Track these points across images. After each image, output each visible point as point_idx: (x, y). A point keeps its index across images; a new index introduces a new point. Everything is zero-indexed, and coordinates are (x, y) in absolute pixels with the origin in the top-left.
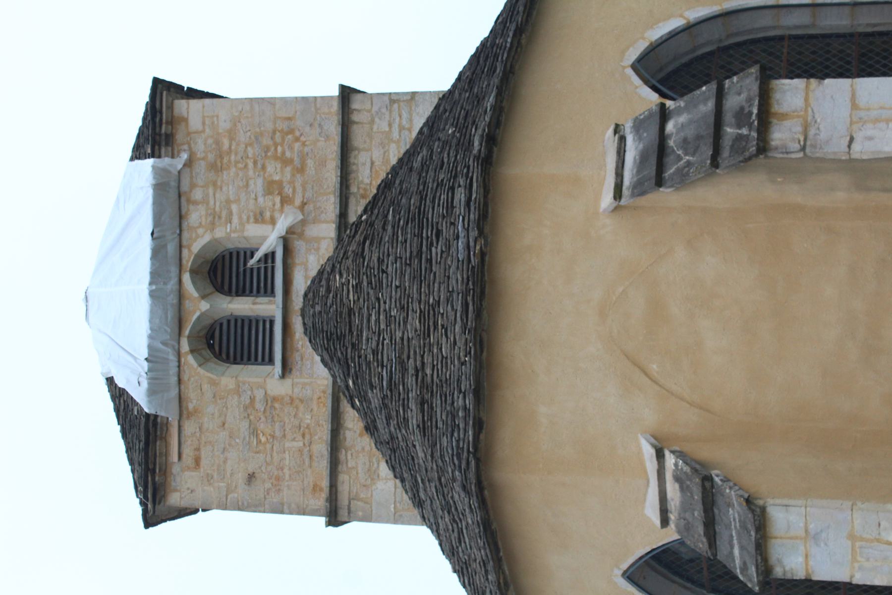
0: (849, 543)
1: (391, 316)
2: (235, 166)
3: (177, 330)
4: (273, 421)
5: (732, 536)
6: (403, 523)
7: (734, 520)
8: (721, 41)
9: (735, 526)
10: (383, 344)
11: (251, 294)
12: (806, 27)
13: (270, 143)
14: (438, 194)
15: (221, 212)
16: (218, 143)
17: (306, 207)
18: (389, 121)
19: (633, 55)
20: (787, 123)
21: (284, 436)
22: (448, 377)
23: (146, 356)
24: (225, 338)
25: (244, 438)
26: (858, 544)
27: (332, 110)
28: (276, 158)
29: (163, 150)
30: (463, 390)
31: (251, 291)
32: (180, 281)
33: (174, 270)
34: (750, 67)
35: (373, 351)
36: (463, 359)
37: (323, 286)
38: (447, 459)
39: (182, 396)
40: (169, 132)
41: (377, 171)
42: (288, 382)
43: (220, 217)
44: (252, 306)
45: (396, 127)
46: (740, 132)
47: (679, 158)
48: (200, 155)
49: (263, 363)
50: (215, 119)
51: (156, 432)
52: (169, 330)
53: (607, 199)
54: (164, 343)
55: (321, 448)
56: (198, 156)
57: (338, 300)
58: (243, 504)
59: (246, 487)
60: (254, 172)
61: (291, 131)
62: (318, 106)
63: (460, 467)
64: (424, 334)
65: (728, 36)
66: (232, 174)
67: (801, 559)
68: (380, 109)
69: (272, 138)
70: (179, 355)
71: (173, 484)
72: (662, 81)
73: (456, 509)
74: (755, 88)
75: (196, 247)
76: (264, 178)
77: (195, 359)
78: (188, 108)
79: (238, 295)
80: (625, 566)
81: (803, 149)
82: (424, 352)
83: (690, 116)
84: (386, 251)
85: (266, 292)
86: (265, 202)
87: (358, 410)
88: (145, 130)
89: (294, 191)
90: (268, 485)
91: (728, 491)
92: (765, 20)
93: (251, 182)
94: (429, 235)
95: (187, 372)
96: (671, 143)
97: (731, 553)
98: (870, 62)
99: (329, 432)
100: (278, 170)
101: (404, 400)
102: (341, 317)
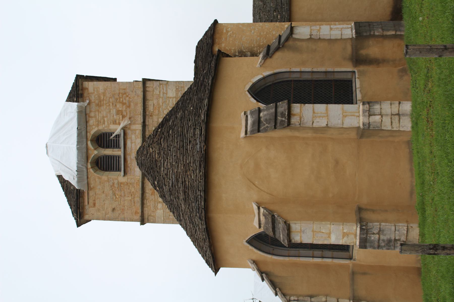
0: (312, 233)
1: (172, 164)
2: (106, 105)
3: (86, 161)
4: (121, 191)
5: (280, 232)
6: (166, 223)
7: (281, 227)
8: (273, 81)
10: (169, 173)
11: (111, 148)
12: (298, 78)
13: (118, 97)
14: (189, 130)
15: (101, 120)
16: (99, 97)
17: (131, 119)
18: (159, 91)
19: (248, 87)
20: (295, 117)
21: (125, 196)
22: (194, 185)
23: (76, 170)
24: (102, 163)
25: (111, 197)
26: (315, 233)
27: (139, 87)
28: (120, 102)
30: (200, 190)
31: (111, 147)
32: (87, 144)
33: (85, 140)
34: (285, 100)
35: (166, 174)
36: (200, 181)
37: (145, 151)
38: (194, 210)
39: (89, 183)
40: (82, 93)
41: (155, 107)
42: (126, 178)
43: (101, 122)
44: (112, 152)
45: (162, 93)
46: (282, 119)
47: (264, 125)
48: (93, 101)
49: (116, 171)
50: (98, 89)
51: (80, 195)
52: (84, 161)
53: (243, 134)
54: (82, 165)
55: (138, 199)
56: (92, 101)
57: (151, 156)
58: (111, 218)
59: (112, 213)
60: (112, 107)
61: (125, 93)
62: (134, 85)
63: (199, 212)
64: (185, 171)
65: (275, 80)
66: (104, 108)
67: (299, 238)
68: (156, 87)
69: (118, 96)
70: (87, 169)
71: (86, 212)
72: (255, 95)
73: (196, 224)
74: (286, 107)
75: (92, 132)
76: (116, 109)
77: (93, 170)
78: (88, 85)
79: (106, 148)
80: (247, 239)
81: (300, 124)
82: (185, 177)
83: (267, 112)
84: (170, 144)
85: (116, 147)
86: (116, 117)
88: (73, 92)
90: (120, 212)
91: (279, 219)
92: (286, 75)
93: (111, 110)
94: (187, 141)
95: (90, 174)
96: (262, 119)
97: (280, 236)
98: (317, 90)
99: (141, 194)
100: (121, 106)
101: (178, 190)
102: (152, 162)
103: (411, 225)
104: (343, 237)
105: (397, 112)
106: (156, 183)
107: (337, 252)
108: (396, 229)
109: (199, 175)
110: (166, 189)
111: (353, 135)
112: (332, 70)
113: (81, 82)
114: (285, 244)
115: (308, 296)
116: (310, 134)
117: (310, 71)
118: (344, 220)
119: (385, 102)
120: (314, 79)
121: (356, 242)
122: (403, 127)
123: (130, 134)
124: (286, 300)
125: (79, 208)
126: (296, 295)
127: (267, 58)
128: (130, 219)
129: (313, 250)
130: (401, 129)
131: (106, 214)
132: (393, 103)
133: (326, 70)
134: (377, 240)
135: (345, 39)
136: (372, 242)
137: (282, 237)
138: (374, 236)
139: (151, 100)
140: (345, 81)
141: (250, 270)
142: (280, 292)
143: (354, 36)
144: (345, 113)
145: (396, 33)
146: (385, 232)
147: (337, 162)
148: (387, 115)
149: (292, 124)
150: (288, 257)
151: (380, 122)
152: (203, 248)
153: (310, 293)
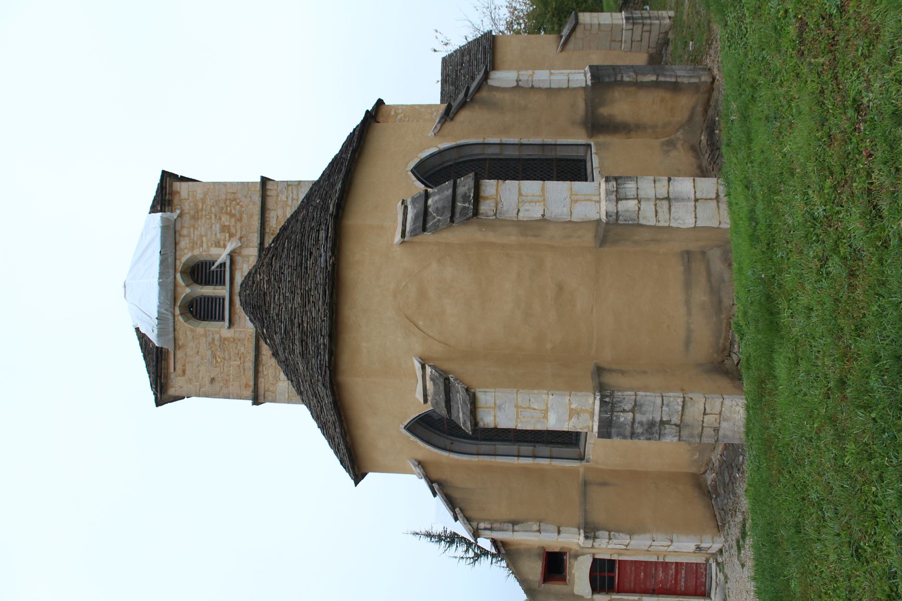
2: (205, 217)
4: (224, 351)
8: (456, 159)
9: (460, 402)
11: (212, 284)
13: (224, 205)
16: (196, 205)
19: (412, 165)
20: (488, 202)
21: (230, 358)
23: (157, 316)
26: (520, 410)
28: (226, 213)
29: (167, 209)
31: (213, 283)
33: (172, 271)
34: (470, 173)
35: (277, 314)
40: (170, 199)
41: (280, 221)
42: (232, 330)
43: (197, 244)
45: (290, 198)
47: (434, 218)
48: (186, 211)
53: (398, 238)
54: (166, 310)
55: (250, 365)
61: (235, 200)
66: (203, 221)
67: (492, 418)
68: (282, 189)
70: (174, 316)
71: (171, 383)
73: (320, 396)
74: (472, 183)
75: (184, 259)
76: (221, 224)
77: (182, 317)
78: (180, 187)
80: (406, 423)
81: (495, 214)
87: (269, 345)
88: (157, 198)
89: (236, 229)
90: (221, 384)
92: (477, 151)
93: (214, 226)
96: (430, 210)
97: (458, 415)
100: (228, 220)
103: (690, 395)
104: (570, 417)
105: (666, 196)
106: (265, 331)
107: (558, 447)
108: (664, 402)
109: (322, 308)
110: (277, 338)
111: (588, 237)
112: (553, 143)
113: (169, 182)
114: (467, 429)
115: (509, 522)
116: (513, 238)
117: (517, 142)
118: (572, 387)
119: (645, 177)
120: (523, 157)
121: (593, 426)
122: (676, 220)
123: (240, 262)
124: (471, 528)
125: (161, 377)
126: (489, 520)
127: (446, 120)
128: (237, 395)
129: (519, 444)
130: (673, 224)
131: (201, 387)
132: (659, 180)
133: (543, 141)
134: (630, 423)
135: (574, 89)
136: (621, 426)
137: (461, 417)
138: (625, 416)
139: (273, 210)
140: (574, 160)
141: (414, 477)
142: (461, 514)
143: (589, 83)
144: (575, 196)
145: (657, 79)
146: (644, 409)
147: (560, 288)
148: (648, 199)
149: (482, 214)
150: (476, 456)
151: (635, 211)
152: (334, 438)
153: (513, 517)
